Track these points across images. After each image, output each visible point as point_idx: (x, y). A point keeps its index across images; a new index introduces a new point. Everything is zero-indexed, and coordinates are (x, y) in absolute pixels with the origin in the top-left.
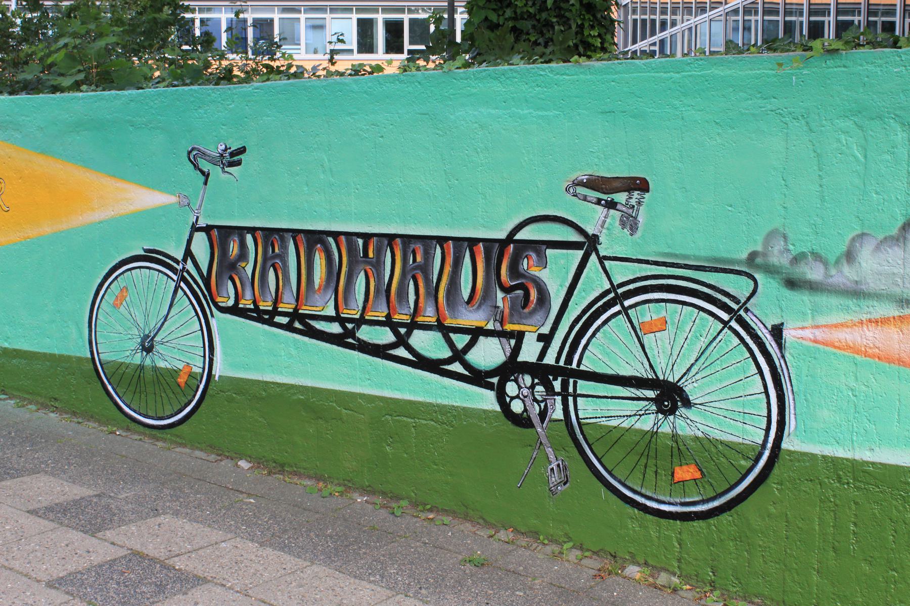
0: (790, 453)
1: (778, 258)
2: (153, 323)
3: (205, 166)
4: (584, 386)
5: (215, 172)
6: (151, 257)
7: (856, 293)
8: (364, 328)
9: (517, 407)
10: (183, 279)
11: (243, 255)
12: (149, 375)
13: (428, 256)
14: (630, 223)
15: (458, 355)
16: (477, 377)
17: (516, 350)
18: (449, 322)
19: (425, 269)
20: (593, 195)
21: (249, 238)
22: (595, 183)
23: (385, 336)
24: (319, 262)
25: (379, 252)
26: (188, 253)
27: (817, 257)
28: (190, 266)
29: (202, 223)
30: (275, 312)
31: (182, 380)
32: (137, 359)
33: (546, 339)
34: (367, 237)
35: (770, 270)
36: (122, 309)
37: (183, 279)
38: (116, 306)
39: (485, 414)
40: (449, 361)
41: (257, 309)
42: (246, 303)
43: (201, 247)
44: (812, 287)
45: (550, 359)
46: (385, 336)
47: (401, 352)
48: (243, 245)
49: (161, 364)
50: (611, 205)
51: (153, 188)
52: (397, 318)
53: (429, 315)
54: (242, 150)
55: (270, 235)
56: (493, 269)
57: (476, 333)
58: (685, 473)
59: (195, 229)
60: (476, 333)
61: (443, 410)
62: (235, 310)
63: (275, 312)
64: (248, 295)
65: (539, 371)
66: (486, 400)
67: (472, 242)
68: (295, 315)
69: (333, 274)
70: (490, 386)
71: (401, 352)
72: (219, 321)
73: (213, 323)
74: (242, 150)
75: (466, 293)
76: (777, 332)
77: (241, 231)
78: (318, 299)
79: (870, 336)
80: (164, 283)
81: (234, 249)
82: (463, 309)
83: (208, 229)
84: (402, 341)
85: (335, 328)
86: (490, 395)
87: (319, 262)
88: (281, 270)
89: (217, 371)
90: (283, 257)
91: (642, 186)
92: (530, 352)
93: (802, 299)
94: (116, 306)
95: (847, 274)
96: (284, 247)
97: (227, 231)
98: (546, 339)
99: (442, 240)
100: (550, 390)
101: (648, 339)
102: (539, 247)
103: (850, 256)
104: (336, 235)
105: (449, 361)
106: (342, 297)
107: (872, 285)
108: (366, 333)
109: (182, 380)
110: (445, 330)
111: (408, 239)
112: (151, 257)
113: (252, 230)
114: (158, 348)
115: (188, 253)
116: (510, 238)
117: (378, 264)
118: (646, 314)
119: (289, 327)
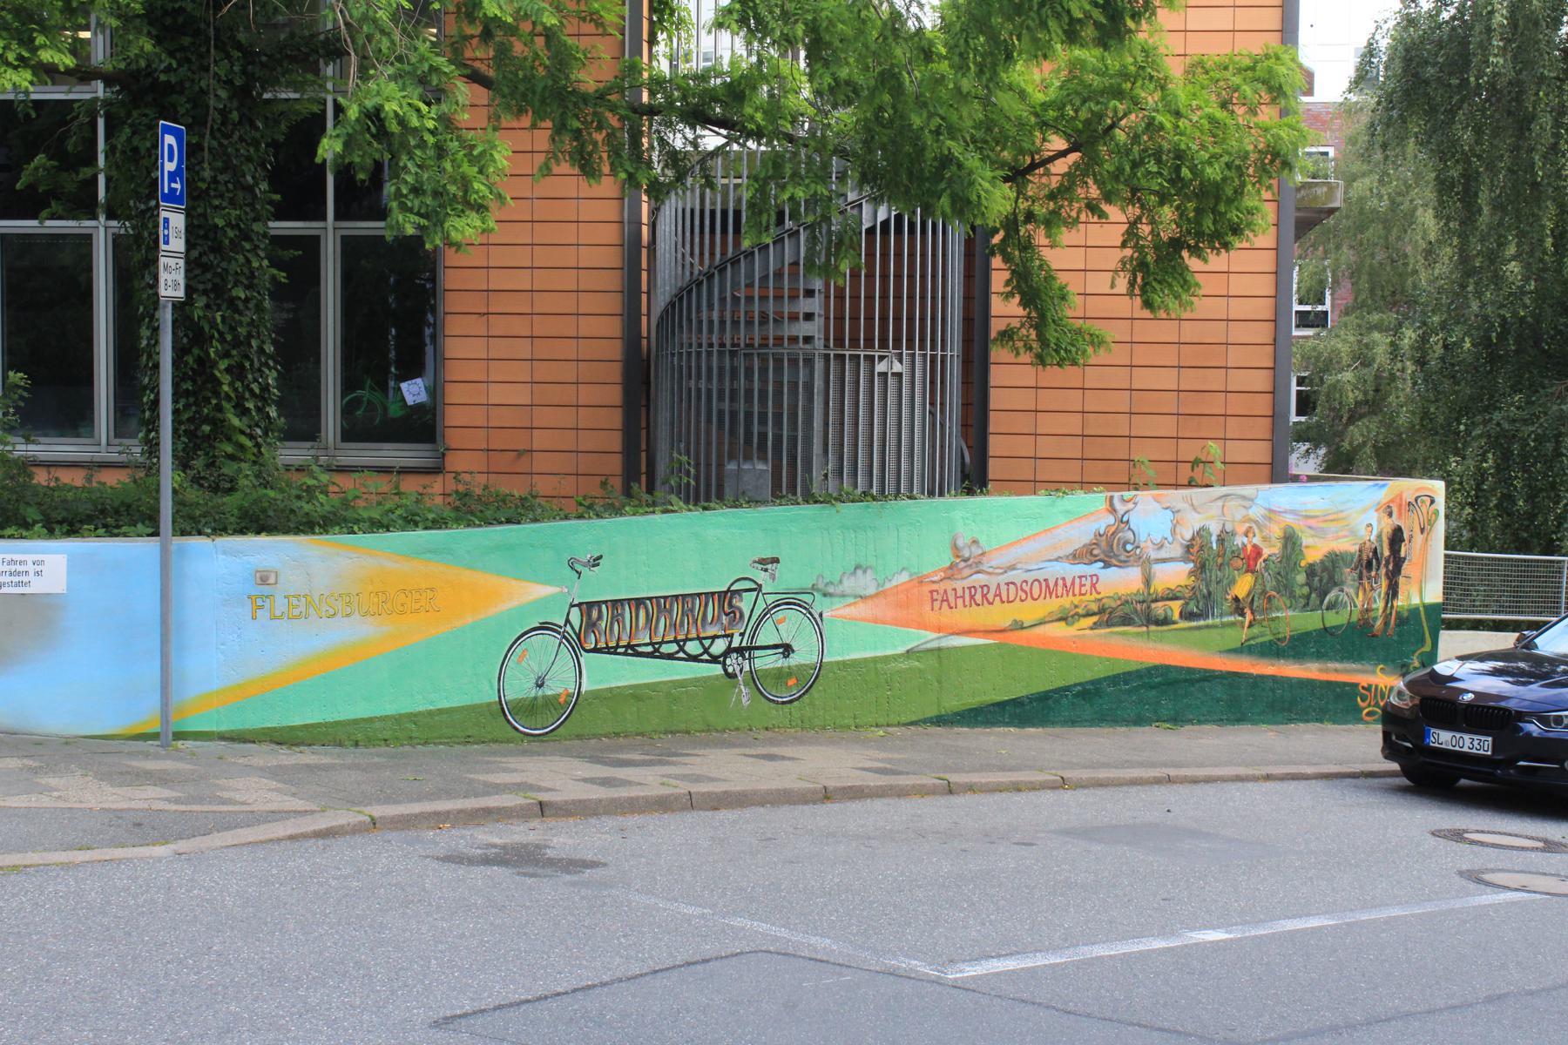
0: (830, 663)
1: (821, 586)
2: (544, 668)
3: (578, 567)
4: (758, 653)
5: (585, 571)
6: (544, 627)
7: (843, 596)
8: (688, 643)
9: (730, 670)
10: (565, 637)
11: (600, 617)
12: (540, 701)
13: (693, 604)
14: (773, 577)
15: (706, 651)
16: (714, 659)
17: (730, 643)
18: (702, 635)
19: (692, 610)
20: (760, 566)
21: (604, 607)
22: (762, 561)
23: (673, 648)
24: (642, 614)
25: (671, 605)
26: (568, 621)
27: (832, 583)
28: (568, 628)
29: (576, 602)
30: (618, 646)
31: (561, 700)
32: (533, 694)
33: (742, 635)
34: (665, 598)
35: (818, 590)
36: (524, 664)
37: (565, 637)
38: (519, 662)
39: (717, 677)
40: (677, 652)
41: (607, 647)
42: (602, 645)
43: (575, 617)
44: (831, 595)
45: (744, 644)
46: (673, 648)
47: (681, 655)
48: (600, 611)
49: (549, 693)
50: (766, 570)
51: (1294, 657)
52: (679, 637)
53: (693, 634)
54: (600, 557)
55: (616, 603)
56: (722, 607)
57: (714, 638)
58: (791, 682)
59: (572, 606)
60: (714, 638)
61: (697, 680)
62: (595, 650)
63: (618, 646)
64: (603, 639)
65: (740, 651)
66: (717, 669)
67: (713, 594)
68: (629, 646)
69: (649, 619)
70: (719, 663)
71: (681, 655)
72: (586, 658)
73: (582, 660)
74: (600, 557)
75: (709, 619)
76: (821, 615)
77: (599, 603)
78: (641, 635)
79: (847, 611)
80: (550, 641)
81: (595, 614)
82: (708, 627)
83: (579, 605)
84: (681, 649)
85: (649, 649)
86: (719, 667)
87: (642, 614)
88: (621, 622)
89: (583, 690)
90: (623, 615)
91: (776, 560)
92: (735, 644)
93: (828, 600)
94: (519, 662)
95: (840, 589)
96: (623, 609)
97: (590, 605)
98: (742, 635)
99: (699, 595)
100: (744, 658)
101: (780, 627)
102: (738, 592)
103: (841, 582)
104: (650, 599)
105: (677, 652)
106: (652, 631)
107: (848, 591)
108: (665, 649)
109: (561, 700)
110: (700, 639)
111: (684, 596)
112: (544, 627)
113: (605, 602)
114: (546, 683)
115: (568, 621)
116: (729, 590)
117: (670, 611)
118: (780, 615)
119: (625, 654)
